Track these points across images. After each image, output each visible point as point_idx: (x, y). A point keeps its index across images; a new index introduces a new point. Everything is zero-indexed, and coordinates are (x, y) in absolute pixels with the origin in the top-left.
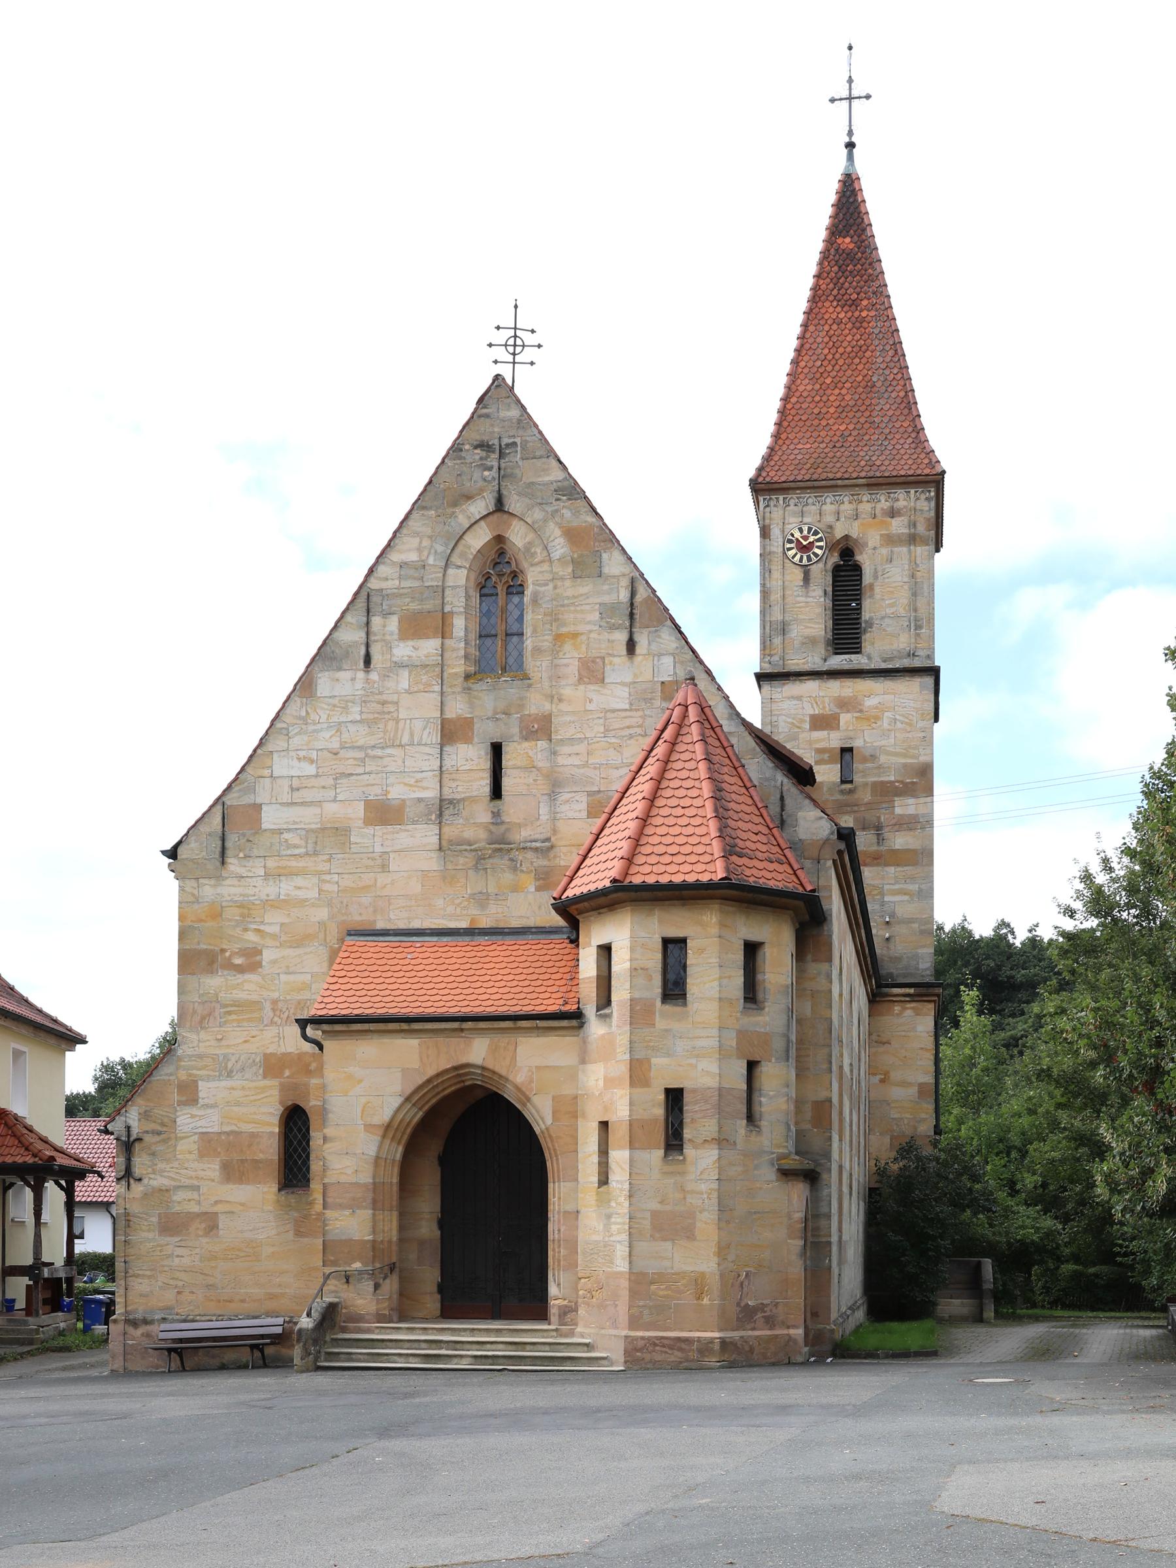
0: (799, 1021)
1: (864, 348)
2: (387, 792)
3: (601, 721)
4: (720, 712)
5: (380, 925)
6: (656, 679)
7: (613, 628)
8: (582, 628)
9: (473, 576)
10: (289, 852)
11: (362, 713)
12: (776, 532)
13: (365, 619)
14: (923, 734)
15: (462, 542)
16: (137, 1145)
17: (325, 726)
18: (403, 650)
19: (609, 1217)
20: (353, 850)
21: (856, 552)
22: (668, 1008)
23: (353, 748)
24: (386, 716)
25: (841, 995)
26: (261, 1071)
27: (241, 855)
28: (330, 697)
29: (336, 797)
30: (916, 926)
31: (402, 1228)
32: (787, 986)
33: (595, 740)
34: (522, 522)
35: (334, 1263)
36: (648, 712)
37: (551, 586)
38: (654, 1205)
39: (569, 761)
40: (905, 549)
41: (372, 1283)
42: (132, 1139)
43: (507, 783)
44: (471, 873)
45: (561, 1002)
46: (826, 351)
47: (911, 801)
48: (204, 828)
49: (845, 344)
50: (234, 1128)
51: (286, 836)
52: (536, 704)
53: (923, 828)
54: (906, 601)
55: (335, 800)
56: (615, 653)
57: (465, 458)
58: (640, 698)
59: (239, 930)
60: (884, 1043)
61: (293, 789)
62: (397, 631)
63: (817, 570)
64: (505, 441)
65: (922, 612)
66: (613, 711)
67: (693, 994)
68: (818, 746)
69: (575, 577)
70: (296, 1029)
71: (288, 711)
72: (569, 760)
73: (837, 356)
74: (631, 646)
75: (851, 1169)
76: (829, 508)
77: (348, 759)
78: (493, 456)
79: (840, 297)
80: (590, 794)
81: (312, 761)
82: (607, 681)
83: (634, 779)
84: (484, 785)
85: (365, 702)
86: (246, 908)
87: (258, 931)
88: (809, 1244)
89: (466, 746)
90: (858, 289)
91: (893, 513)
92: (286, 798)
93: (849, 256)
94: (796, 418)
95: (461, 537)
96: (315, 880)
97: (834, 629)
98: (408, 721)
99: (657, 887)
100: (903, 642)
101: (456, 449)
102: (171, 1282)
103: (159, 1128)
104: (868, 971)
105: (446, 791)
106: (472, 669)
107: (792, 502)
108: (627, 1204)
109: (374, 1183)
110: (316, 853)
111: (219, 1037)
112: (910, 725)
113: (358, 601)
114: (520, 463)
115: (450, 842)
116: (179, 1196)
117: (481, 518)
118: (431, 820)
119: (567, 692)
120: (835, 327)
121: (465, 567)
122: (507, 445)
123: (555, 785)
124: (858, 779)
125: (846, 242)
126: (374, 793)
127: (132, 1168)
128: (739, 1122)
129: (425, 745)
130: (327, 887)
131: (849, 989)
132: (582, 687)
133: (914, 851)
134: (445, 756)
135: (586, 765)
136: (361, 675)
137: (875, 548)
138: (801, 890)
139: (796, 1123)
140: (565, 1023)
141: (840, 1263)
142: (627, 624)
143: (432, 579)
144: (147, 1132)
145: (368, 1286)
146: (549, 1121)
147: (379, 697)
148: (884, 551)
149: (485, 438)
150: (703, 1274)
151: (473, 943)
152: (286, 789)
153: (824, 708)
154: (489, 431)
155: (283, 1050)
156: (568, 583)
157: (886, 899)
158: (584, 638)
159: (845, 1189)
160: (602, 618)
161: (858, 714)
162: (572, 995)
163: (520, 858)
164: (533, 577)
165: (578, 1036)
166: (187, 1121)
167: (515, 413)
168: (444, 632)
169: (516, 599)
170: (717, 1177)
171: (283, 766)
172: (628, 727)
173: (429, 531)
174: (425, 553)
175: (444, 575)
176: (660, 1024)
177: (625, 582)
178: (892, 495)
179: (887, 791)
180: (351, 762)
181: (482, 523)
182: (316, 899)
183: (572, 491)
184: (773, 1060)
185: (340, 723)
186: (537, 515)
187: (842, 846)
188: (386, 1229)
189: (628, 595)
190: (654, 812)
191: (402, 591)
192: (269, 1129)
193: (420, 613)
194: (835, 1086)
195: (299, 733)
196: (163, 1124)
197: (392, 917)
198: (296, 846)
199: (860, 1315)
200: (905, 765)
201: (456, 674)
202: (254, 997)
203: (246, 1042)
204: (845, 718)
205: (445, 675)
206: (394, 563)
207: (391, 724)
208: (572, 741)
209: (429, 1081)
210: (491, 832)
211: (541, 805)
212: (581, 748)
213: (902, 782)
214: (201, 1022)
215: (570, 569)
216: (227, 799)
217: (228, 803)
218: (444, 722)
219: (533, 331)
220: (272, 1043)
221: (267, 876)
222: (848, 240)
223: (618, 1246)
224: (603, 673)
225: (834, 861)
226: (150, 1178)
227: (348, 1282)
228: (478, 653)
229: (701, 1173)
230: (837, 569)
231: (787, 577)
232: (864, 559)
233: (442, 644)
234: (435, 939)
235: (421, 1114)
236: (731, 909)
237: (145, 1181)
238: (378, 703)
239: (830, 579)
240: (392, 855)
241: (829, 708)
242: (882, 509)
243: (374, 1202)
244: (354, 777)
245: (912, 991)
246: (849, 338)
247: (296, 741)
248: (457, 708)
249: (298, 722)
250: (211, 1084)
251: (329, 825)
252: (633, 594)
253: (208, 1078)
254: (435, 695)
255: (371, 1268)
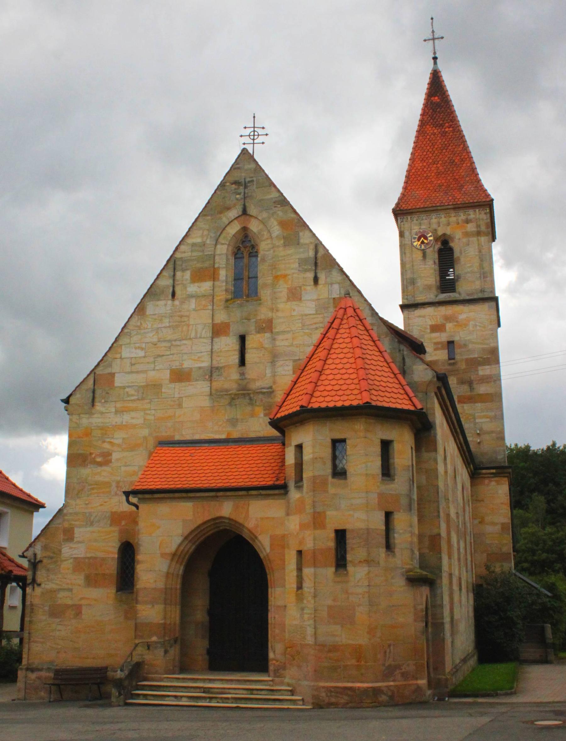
0: (418, 487)
1: (448, 145)
2: (182, 364)
3: (300, 321)
4: (366, 314)
5: (177, 438)
6: (330, 297)
7: (306, 271)
8: (288, 272)
9: (230, 249)
10: (128, 399)
11: (170, 322)
12: (407, 234)
13: (172, 273)
14: (492, 332)
15: (225, 231)
16: (39, 564)
17: (150, 330)
18: (193, 289)
19: (303, 609)
20: (163, 397)
21: (450, 242)
22: (335, 480)
23: (165, 341)
24: (183, 324)
25: (446, 472)
26: (109, 522)
27: (103, 401)
28: (153, 315)
29: (154, 368)
30: (494, 435)
31: (183, 615)
32: (409, 466)
33: (297, 331)
34: (256, 220)
35: (142, 637)
36: (326, 315)
37: (272, 251)
38: (330, 602)
39: (283, 343)
40: (475, 239)
41: (163, 650)
42: (37, 561)
43: (248, 357)
44: (228, 407)
45: (275, 479)
46: (428, 148)
47: (487, 367)
48: (84, 387)
49: (438, 144)
50: (93, 555)
51: (127, 390)
52: (264, 313)
53: (495, 381)
54: (478, 264)
55: (154, 370)
56: (307, 284)
57: (226, 190)
58: (321, 307)
59: (100, 442)
60: (480, 501)
61: (132, 365)
62: (189, 279)
63: (429, 251)
64: (248, 180)
65: (487, 269)
66: (306, 315)
67: (351, 472)
68: (435, 341)
69: (285, 245)
70: (124, 498)
71: (130, 323)
72: (282, 343)
73: (434, 149)
74: (316, 280)
75: (460, 574)
76: (434, 221)
77: (162, 347)
78: (241, 187)
79: (434, 123)
80: (295, 361)
81: (142, 349)
82: (303, 299)
83: (316, 350)
84: (235, 358)
85: (171, 316)
86: (105, 430)
87: (110, 442)
88: (430, 624)
89: (225, 337)
90: (443, 119)
91: (467, 221)
92: (128, 369)
93: (438, 105)
94: (415, 179)
95: (224, 229)
96: (142, 414)
97: (440, 281)
98: (194, 326)
99: (327, 409)
100: (477, 285)
101: (222, 185)
102: (54, 646)
103: (51, 555)
104: (467, 460)
105: (214, 362)
106: (230, 297)
107: (415, 219)
108: (313, 602)
109: (166, 589)
110: (143, 399)
111: (87, 502)
112: (484, 327)
113: (169, 264)
114: (256, 190)
115: (217, 390)
116: (61, 594)
117: (235, 219)
118: (206, 378)
119: (281, 306)
120: (432, 136)
121: (226, 244)
122: (249, 182)
123: (274, 357)
124: (458, 357)
125: (436, 99)
126: (176, 365)
127: (36, 577)
128: (381, 550)
129: (204, 338)
130: (149, 417)
131: (453, 468)
132: (289, 303)
133: (491, 394)
134: (214, 343)
135: (292, 345)
136: (170, 302)
137: (459, 239)
138: (412, 408)
139: (419, 549)
140: (277, 492)
141: (453, 634)
142: (314, 268)
143: (209, 251)
144: (45, 557)
145: (161, 652)
146: (268, 550)
147: (179, 313)
148: (465, 240)
149: (237, 179)
150: (360, 646)
151: (228, 447)
152: (128, 364)
153: (437, 321)
154: (240, 176)
155: (122, 510)
156: (281, 249)
157: (477, 421)
158: (290, 277)
159: (455, 587)
160: (300, 266)
161: (455, 323)
162: (282, 475)
163: (255, 398)
164: (263, 247)
165: (284, 499)
166: (67, 551)
167: (253, 166)
168: (214, 276)
169: (254, 259)
170: (367, 584)
171: (126, 352)
172: (315, 323)
173: (207, 227)
174: (205, 238)
175: (215, 249)
176: (332, 490)
177: (312, 247)
178: (467, 213)
179: (474, 363)
180: (163, 349)
181: (236, 221)
182: (142, 424)
183: (283, 202)
184: (401, 511)
185: (158, 328)
186: (265, 215)
187: (440, 384)
188: (173, 616)
189: (314, 253)
190: (326, 367)
191: (193, 258)
192: (112, 556)
193: (202, 268)
194: (443, 526)
195: (136, 334)
196: (54, 553)
197: (184, 433)
198: (132, 395)
199: (473, 662)
200: (483, 349)
201: (253, 319)
202: (107, 480)
203: (101, 505)
204: (449, 326)
205: (215, 300)
206: (188, 244)
207: (185, 328)
208: (283, 332)
209: (198, 527)
210: (239, 385)
211: (267, 368)
212: (289, 336)
213: (481, 358)
214: (77, 494)
215: (282, 242)
216: (98, 371)
217: (97, 373)
218: (214, 325)
219: (263, 128)
220: (116, 505)
221: (116, 412)
222: (436, 98)
223: (308, 628)
224: (301, 295)
225: (436, 394)
226: (45, 584)
227: (149, 649)
228: (233, 288)
229: (358, 582)
230: (440, 251)
231: (414, 256)
232: (455, 245)
233: (213, 284)
234: (207, 445)
235: (193, 547)
236: (372, 421)
237: (43, 586)
238: (179, 316)
239: (436, 256)
240: (184, 399)
241: (440, 321)
242: (462, 220)
243: (165, 600)
244: (165, 357)
245: (494, 471)
246: (440, 141)
247: (135, 339)
248: (221, 317)
249: (136, 328)
250: (82, 530)
251: (150, 383)
252: (316, 252)
253: (80, 526)
254: (208, 311)
255: (163, 640)
